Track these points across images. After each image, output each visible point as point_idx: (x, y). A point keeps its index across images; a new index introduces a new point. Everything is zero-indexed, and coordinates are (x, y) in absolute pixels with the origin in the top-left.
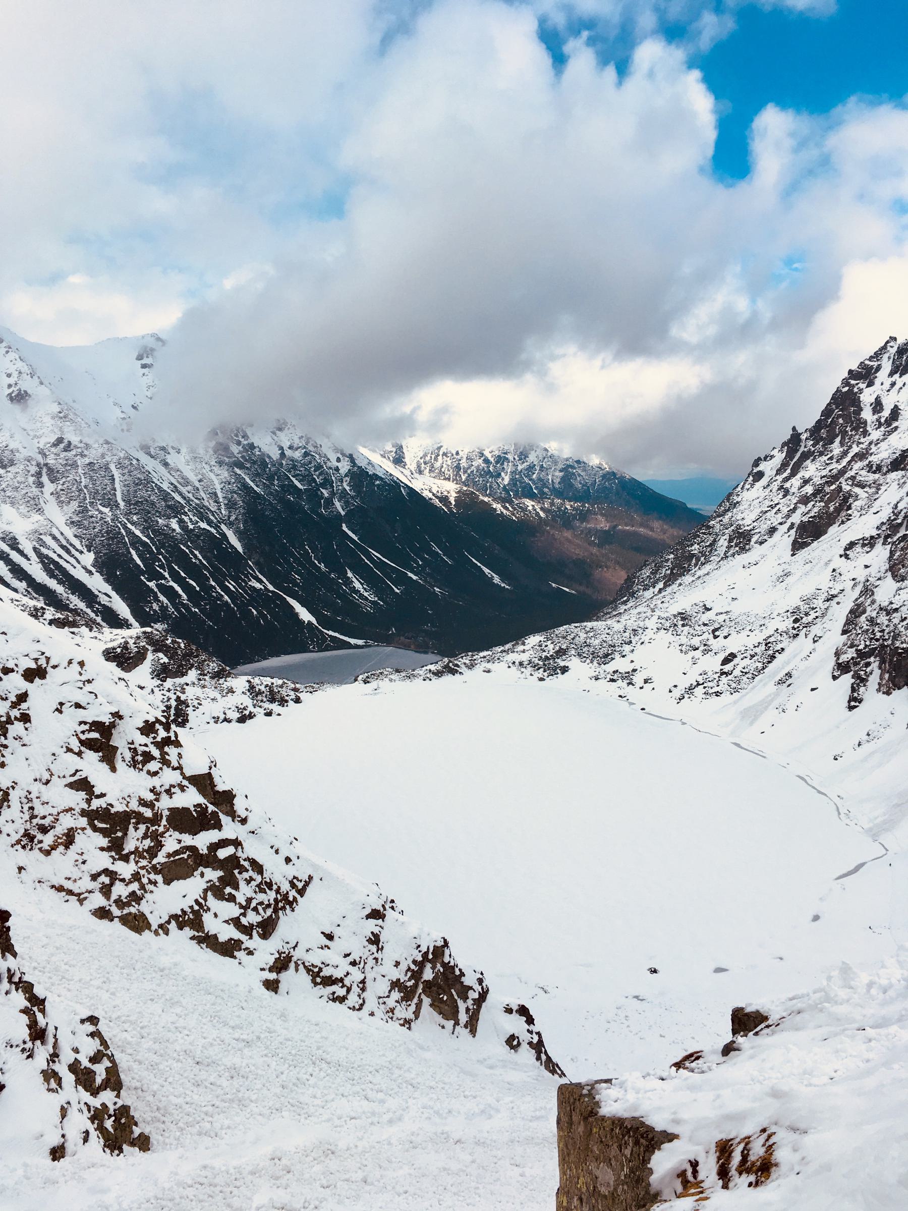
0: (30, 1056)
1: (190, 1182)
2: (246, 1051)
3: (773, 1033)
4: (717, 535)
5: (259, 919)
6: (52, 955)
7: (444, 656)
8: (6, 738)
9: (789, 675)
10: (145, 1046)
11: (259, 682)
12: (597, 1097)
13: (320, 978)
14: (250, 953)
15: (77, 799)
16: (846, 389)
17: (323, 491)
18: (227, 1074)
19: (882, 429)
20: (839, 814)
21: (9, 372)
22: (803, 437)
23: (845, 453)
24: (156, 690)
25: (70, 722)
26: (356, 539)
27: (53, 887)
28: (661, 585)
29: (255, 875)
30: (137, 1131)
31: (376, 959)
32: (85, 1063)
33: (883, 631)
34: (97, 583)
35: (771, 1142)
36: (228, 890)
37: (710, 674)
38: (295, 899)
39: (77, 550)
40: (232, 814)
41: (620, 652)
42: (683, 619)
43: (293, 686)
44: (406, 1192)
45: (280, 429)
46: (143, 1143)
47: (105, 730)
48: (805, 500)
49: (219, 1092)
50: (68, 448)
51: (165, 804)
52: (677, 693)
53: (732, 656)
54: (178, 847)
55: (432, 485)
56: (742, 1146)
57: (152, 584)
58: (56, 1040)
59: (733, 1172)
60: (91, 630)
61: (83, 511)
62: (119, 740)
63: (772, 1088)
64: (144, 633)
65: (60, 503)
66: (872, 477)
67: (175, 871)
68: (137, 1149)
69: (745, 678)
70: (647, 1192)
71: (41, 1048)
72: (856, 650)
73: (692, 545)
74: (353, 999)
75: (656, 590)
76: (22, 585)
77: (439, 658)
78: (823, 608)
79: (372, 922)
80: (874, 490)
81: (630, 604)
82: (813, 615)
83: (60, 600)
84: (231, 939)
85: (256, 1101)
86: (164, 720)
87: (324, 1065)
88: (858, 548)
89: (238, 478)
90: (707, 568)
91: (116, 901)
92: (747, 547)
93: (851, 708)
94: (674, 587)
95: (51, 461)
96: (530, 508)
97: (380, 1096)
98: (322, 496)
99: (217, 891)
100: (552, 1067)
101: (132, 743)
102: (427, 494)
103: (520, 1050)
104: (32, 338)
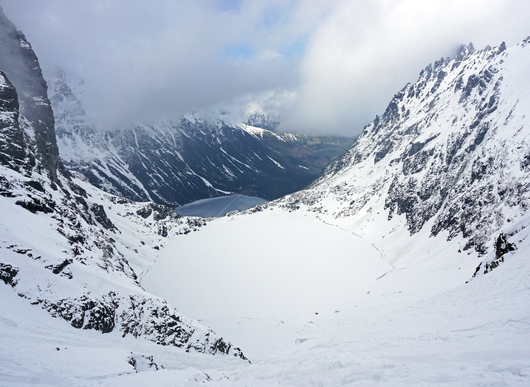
9: (371, 208)
13: (196, 348)
22: (380, 118)
23: (392, 127)
28: (333, 173)
34: (130, 176)
41: (317, 201)
42: (338, 188)
48: (379, 143)
51: (167, 322)
52: (335, 215)
53: (354, 201)
57: (150, 175)
61: (124, 149)
62: (158, 313)
65: (115, 146)
66: (400, 136)
67: (169, 334)
81: (323, 180)
82: (379, 187)
88: (394, 163)
90: (348, 168)
93: (389, 220)
95: (111, 130)
99: (177, 336)
102: (252, 133)
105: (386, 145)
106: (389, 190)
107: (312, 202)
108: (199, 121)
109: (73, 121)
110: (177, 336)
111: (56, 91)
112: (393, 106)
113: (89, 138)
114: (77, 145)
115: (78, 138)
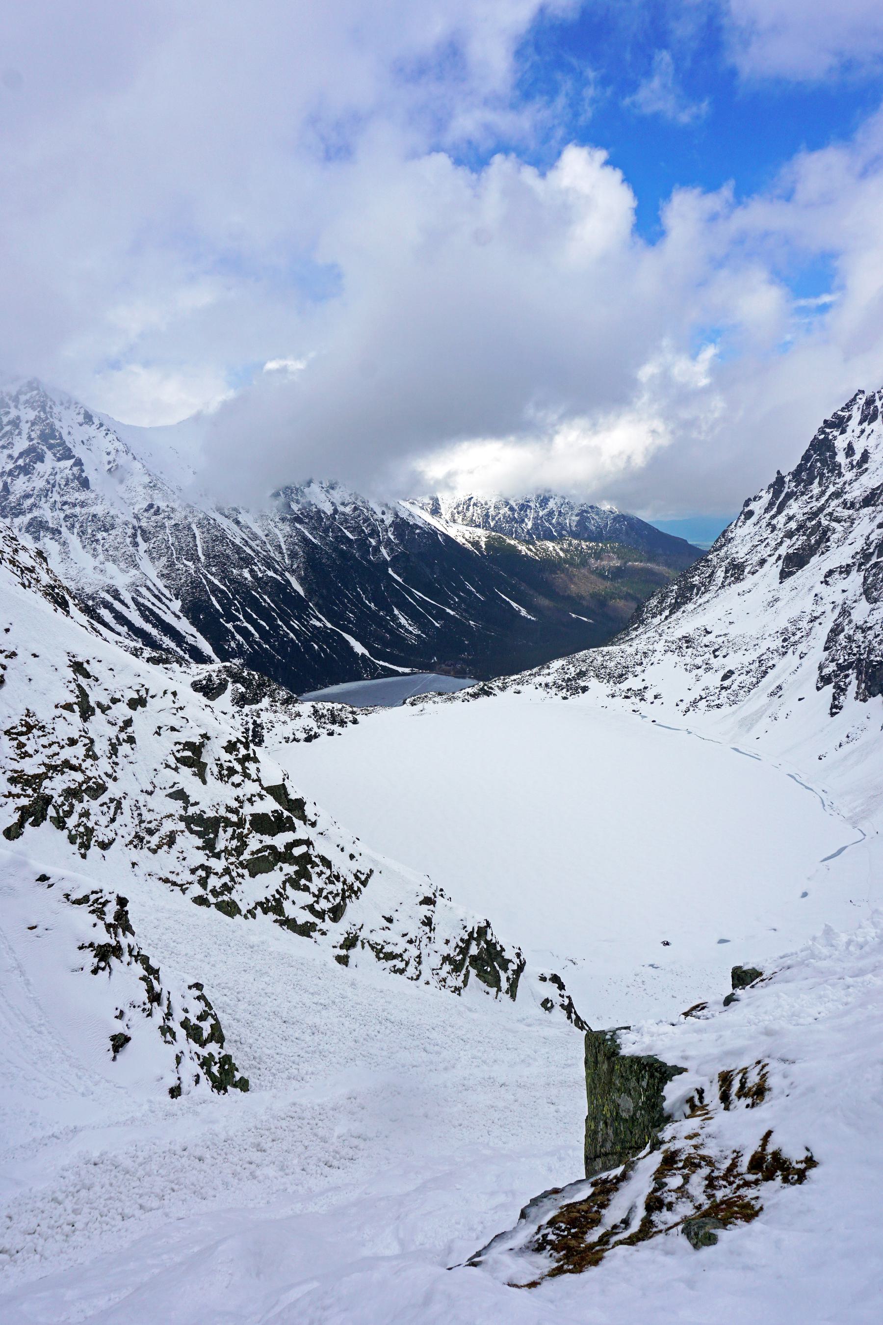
0: (149, 1015)
1: (283, 1116)
2: (324, 1012)
3: (767, 985)
4: (715, 567)
5: (330, 905)
6: (163, 934)
7: (479, 680)
8: (117, 757)
9: (780, 687)
10: (242, 1007)
11: (322, 707)
12: (618, 1041)
13: (382, 954)
14: (324, 933)
15: (176, 806)
16: (822, 436)
17: (371, 540)
18: (309, 1031)
19: (854, 470)
20: (824, 806)
21: (108, 450)
22: (787, 480)
23: (823, 493)
24: (236, 715)
25: (168, 741)
26: (400, 580)
27: (160, 879)
28: (667, 613)
29: (325, 870)
30: (238, 1075)
31: (429, 938)
32: (194, 1021)
33: (859, 647)
34: (184, 626)
35: (764, 1071)
36: (303, 882)
37: (711, 689)
38: (359, 889)
39: (167, 598)
40: (304, 818)
41: (633, 672)
42: (687, 642)
43: (350, 709)
44: (460, 1125)
45: (333, 488)
46: (243, 1085)
47: (196, 749)
48: (790, 535)
49: (303, 1045)
50: (157, 513)
51: (248, 810)
52: (683, 706)
53: (731, 672)
54: (260, 846)
55: (465, 532)
56: (740, 1075)
57: (229, 626)
58: (170, 1002)
59: (733, 1097)
60: (181, 666)
61: (171, 565)
62: (207, 758)
63: (766, 1028)
64: (225, 667)
65: (152, 559)
66: (847, 513)
67: (260, 865)
68: (239, 1090)
69: (742, 692)
70: (661, 1115)
71: (158, 1008)
72: (837, 664)
73: (693, 577)
74: (411, 971)
75: (663, 617)
76: (124, 630)
77: (475, 682)
78: (807, 628)
79: (425, 907)
80: (848, 524)
81: (641, 630)
82: (799, 634)
83: (155, 642)
84: (308, 922)
85: (334, 1053)
86: (244, 740)
87: (389, 1024)
88: (836, 575)
89: (299, 532)
90: (707, 596)
91: (211, 891)
92: (741, 577)
93: (833, 714)
94: (679, 614)
95: (144, 524)
96: (551, 549)
97: (437, 1048)
98: (370, 545)
100: (580, 1023)
101: (219, 760)
102: (460, 540)
103: (554, 1011)
104: (126, 421)
105: (811, 534)
106: (828, 641)
107: (621, 676)
108: (341, 509)
109: (65, 503)
110: (296, 886)
111: (32, 440)
112: (822, 447)
113: (97, 541)
114: (71, 556)
115: (74, 541)
